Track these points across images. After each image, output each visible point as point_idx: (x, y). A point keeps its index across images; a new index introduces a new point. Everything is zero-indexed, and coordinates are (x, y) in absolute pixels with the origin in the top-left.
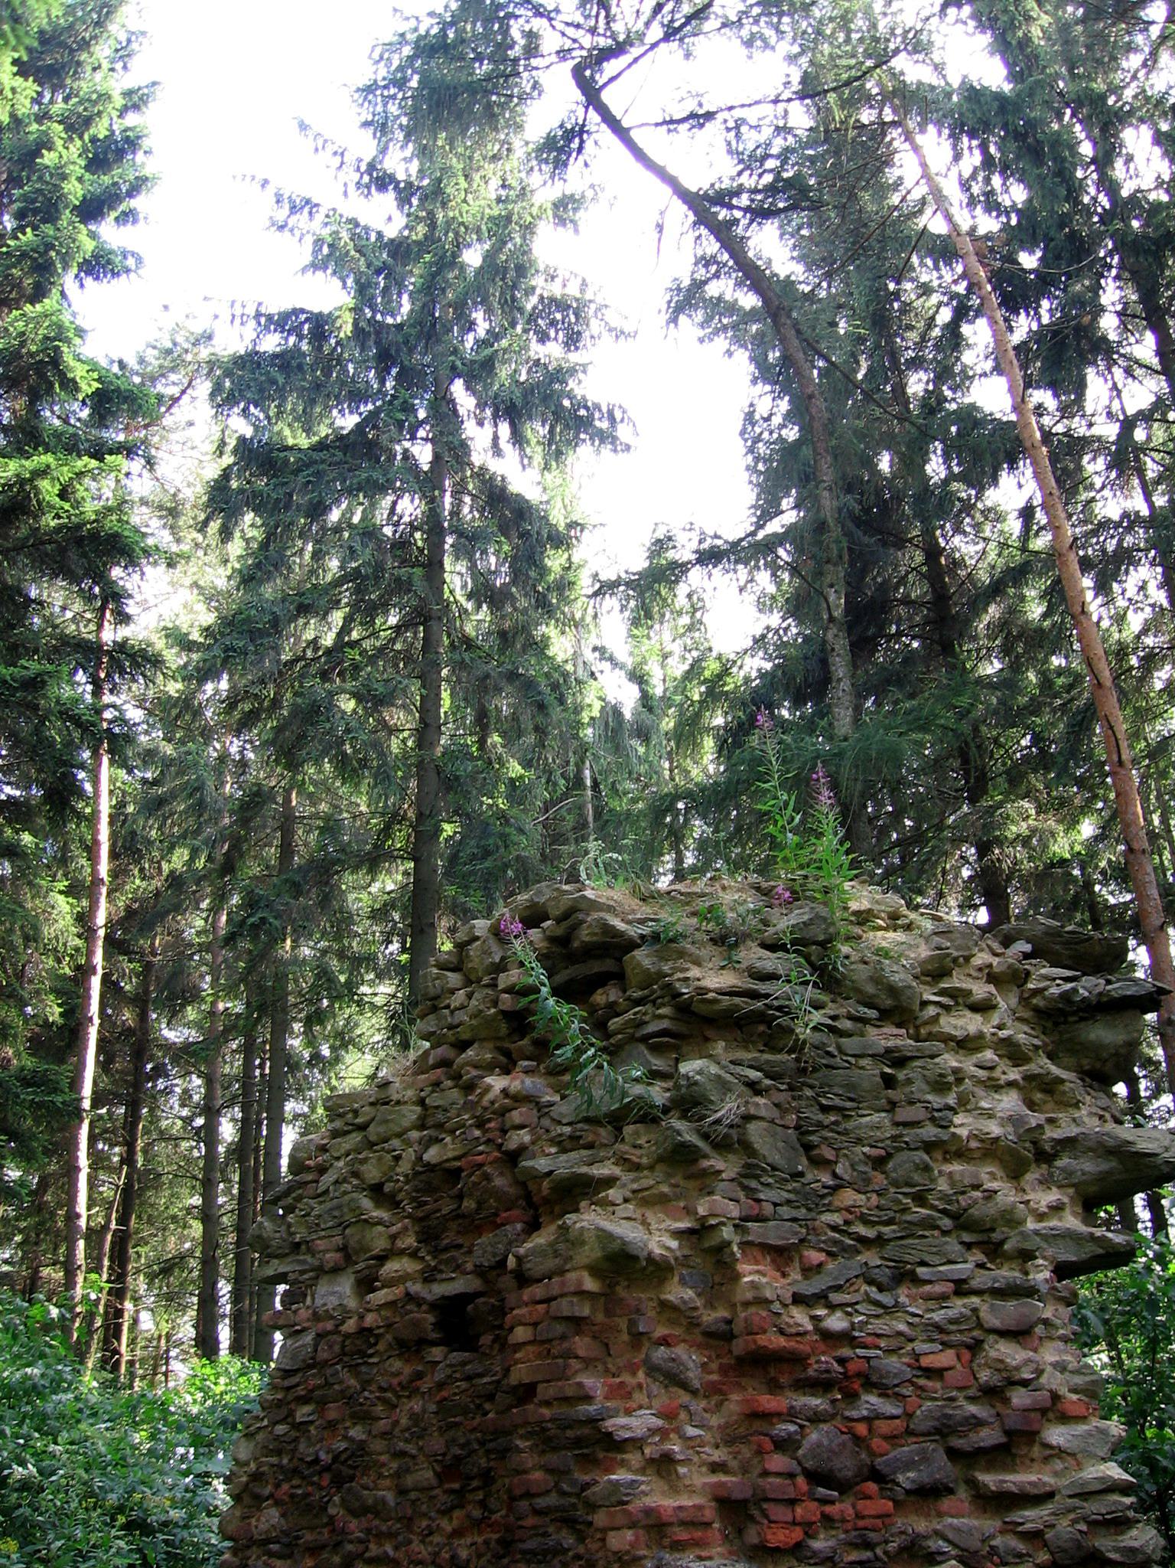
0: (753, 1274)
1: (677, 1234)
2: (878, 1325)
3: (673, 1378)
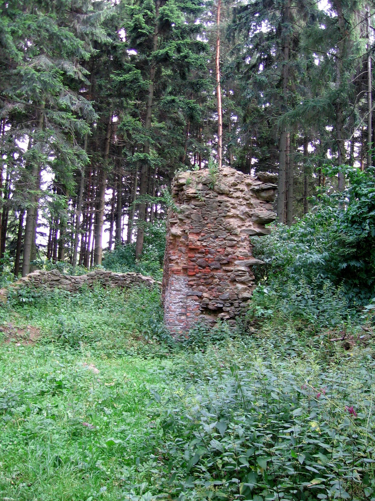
1: (181, 231)
2: (211, 245)
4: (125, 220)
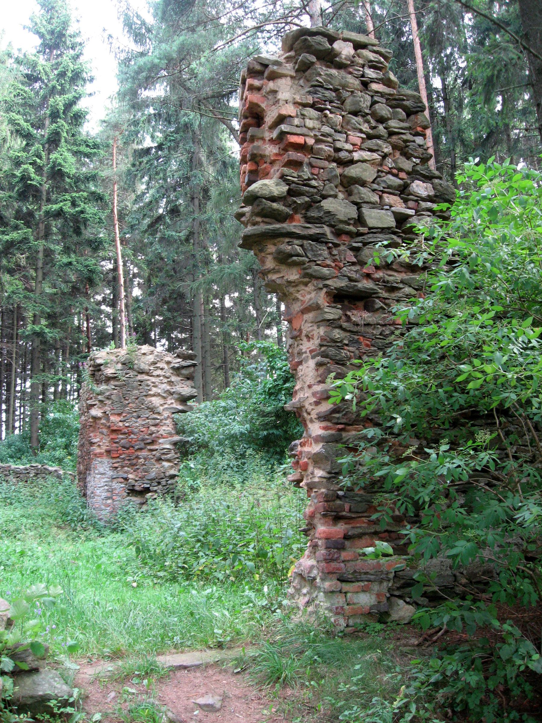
0: (112, 418)
3: (102, 433)
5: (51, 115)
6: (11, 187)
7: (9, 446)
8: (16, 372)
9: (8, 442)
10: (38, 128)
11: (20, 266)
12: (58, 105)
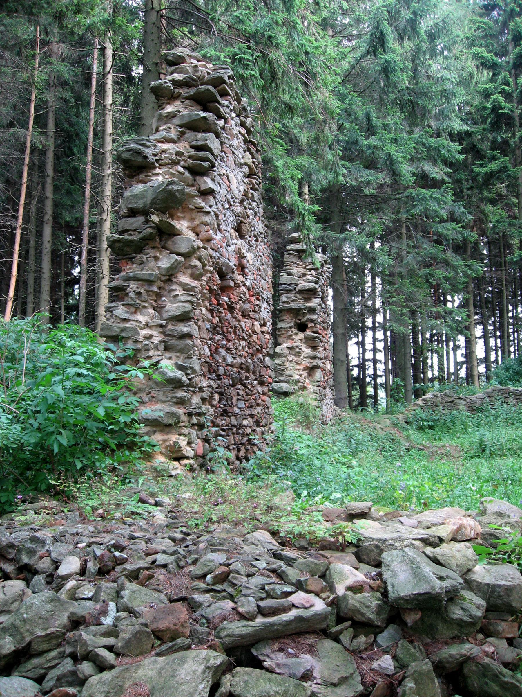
4: (478, 331)
5: (513, 40)
6: (484, 120)
7: (507, 369)
8: (507, 298)
9: (506, 366)
10: (501, 57)
11: (501, 195)
12: (519, 27)
